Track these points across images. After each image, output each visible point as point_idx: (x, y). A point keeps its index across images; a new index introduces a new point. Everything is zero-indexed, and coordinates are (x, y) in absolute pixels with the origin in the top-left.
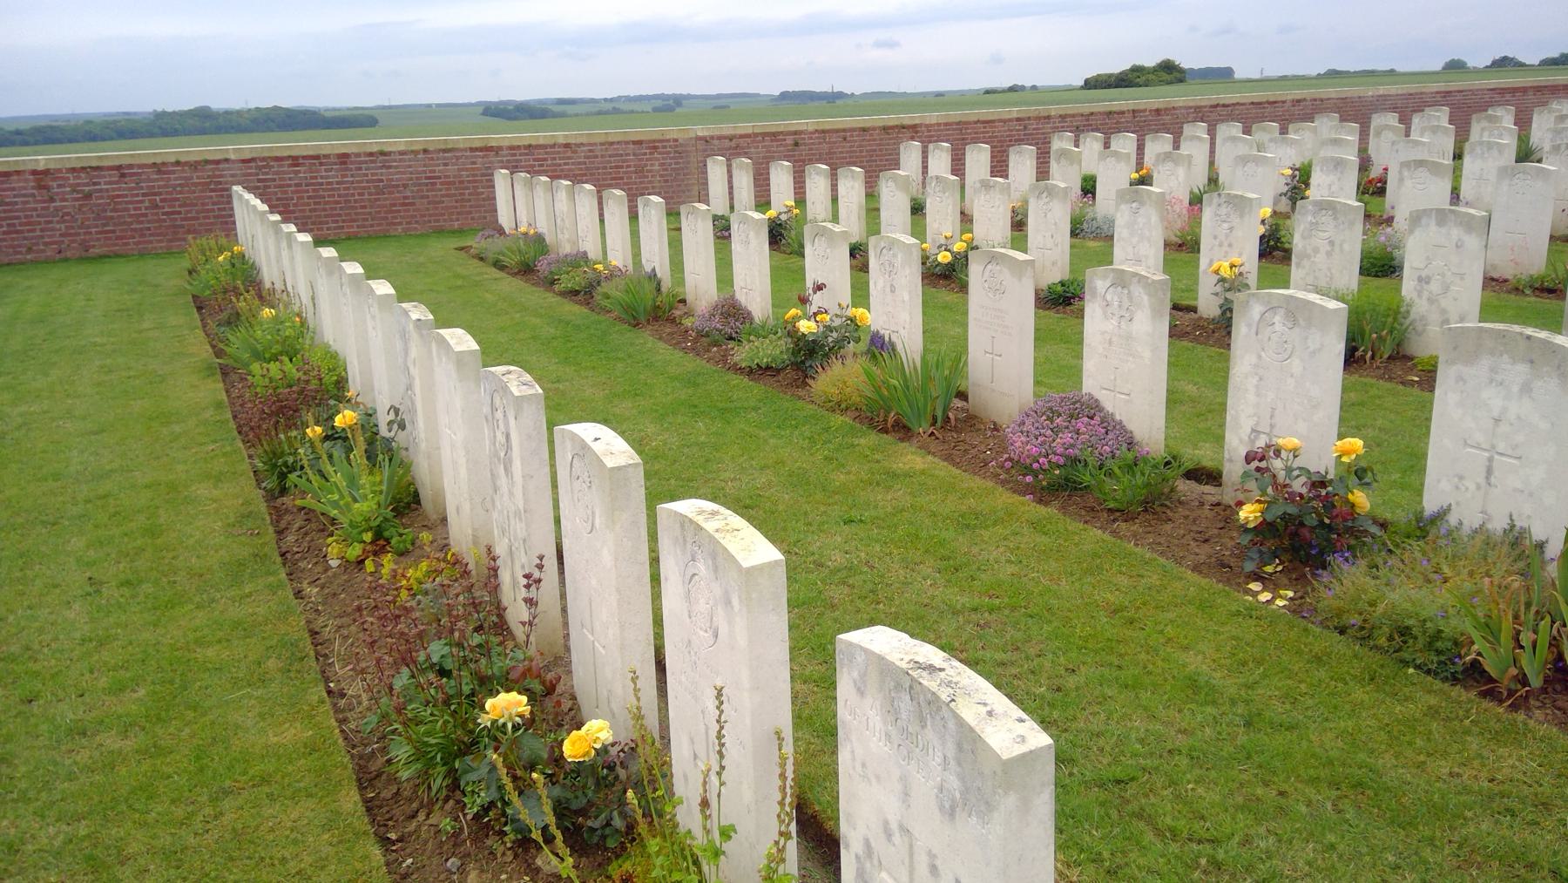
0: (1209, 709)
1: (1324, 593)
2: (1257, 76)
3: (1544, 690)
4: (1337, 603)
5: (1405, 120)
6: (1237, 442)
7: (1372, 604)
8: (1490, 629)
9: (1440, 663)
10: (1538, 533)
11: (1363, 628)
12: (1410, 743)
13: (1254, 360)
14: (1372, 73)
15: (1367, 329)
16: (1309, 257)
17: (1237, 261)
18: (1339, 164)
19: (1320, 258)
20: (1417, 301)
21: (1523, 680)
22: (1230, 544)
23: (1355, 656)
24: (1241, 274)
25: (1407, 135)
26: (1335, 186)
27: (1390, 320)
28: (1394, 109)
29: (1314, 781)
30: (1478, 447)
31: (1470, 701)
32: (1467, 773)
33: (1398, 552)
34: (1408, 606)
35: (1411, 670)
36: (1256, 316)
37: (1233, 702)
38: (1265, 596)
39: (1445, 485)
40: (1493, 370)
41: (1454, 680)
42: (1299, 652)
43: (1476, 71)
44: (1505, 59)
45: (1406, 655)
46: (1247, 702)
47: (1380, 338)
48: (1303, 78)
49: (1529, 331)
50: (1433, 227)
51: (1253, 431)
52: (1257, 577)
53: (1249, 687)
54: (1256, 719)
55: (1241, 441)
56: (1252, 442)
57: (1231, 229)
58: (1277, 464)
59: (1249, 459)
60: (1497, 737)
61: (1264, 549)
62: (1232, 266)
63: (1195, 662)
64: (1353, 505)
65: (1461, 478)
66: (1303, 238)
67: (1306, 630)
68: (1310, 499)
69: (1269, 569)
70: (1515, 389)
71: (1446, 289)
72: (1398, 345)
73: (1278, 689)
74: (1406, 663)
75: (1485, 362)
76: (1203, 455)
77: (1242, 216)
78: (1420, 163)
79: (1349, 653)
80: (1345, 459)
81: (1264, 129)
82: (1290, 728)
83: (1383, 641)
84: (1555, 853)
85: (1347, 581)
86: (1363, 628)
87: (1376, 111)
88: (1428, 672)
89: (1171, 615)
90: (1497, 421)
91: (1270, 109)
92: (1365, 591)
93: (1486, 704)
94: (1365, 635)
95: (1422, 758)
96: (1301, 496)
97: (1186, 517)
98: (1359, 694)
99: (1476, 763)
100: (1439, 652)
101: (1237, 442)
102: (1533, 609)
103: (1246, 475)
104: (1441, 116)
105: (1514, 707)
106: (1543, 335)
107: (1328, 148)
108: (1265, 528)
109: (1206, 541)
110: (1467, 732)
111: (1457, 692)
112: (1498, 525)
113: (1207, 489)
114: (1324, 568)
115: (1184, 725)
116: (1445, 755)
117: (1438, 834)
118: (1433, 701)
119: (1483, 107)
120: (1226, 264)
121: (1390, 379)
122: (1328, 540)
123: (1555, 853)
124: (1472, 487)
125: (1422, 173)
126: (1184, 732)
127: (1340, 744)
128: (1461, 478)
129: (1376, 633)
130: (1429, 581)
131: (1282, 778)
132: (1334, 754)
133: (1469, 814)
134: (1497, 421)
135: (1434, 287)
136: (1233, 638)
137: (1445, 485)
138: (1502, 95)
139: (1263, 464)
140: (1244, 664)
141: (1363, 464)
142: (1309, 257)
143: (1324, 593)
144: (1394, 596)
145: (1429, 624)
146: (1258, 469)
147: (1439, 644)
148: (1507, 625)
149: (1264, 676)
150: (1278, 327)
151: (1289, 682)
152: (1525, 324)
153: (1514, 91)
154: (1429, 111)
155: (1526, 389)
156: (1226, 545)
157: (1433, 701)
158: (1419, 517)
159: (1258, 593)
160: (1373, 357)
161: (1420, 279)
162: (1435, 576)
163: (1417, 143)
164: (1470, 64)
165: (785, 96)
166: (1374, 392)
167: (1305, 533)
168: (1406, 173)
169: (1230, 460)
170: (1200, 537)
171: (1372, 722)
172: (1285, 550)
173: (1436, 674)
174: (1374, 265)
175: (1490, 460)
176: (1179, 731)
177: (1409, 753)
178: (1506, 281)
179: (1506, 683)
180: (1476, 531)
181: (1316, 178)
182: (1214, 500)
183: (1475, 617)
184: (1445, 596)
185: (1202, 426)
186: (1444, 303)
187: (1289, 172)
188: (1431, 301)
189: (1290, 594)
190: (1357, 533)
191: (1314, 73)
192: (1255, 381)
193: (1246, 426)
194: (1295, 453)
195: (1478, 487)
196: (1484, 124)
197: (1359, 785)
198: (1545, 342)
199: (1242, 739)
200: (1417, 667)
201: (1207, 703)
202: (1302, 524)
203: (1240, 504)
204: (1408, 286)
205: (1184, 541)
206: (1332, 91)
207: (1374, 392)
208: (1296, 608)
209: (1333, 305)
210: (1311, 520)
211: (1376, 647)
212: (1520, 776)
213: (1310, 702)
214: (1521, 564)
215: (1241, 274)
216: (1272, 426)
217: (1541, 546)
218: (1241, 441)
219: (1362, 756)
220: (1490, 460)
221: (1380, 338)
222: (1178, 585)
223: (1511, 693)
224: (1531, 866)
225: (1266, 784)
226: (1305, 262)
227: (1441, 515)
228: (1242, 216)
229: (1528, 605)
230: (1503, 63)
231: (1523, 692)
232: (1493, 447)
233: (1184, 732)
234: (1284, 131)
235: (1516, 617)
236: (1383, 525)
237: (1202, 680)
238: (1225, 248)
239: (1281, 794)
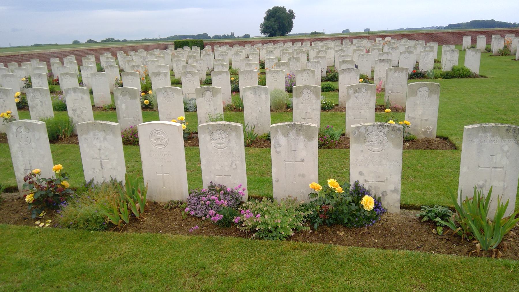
0: (27, 270)
1: (60, 217)
2: (9, 46)
3: (130, 223)
4: (65, 219)
5: (61, 60)
6: (20, 175)
7: (76, 215)
8: (111, 211)
9: (100, 226)
10: (119, 179)
11: (75, 224)
12: (95, 254)
13: (18, 145)
14: (50, 45)
15: (60, 128)
16: (35, 107)
17: (9, 112)
18: (40, 76)
19: (39, 107)
20: (74, 117)
21: (124, 222)
22: (26, 211)
23: (74, 233)
24: (12, 116)
25: (63, 64)
26: (41, 84)
27: (67, 124)
28: (57, 57)
29: (68, 278)
30: (96, 159)
31: (111, 234)
32: (114, 255)
33: (81, 197)
34: (86, 212)
35: (92, 232)
36: (15, 131)
37: (36, 264)
38: (42, 224)
39: (90, 172)
40: (94, 135)
41: (106, 229)
42: (56, 239)
43: (83, 44)
44: (90, 40)
45: (90, 228)
46: (41, 262)
47: (65, 130)
48: (26, 47)
49: (101, 122)
50: (73, 94)
51: (25, 170)
52: (38, 219)
53: (41, 257)
54: (45, 266)
55: (21, 174)
56: (26, 173)
57: (4, 101)
58: (35, 179)
59: (25, 180)
60: (120, 242)
61: (38, 209)
62: (8, 114)
63: (20, 256)
64: (64, 186)
65: (94, 169)
66: (31, 101)
67: (57, 231)
68: (49, 188)
69: (41, 215)
70: (102, 139)
71: (82, 112)
72: (72, 132)
73: (50, 254)
74: (90, 230)
75: (92, 133)
76: (11, 183)
77: (7, 96)
78: (67, 74)
79: (72, 233)
80: (57, 172)
81: (12, 65)
82: (57, 265)
83: (82, 226)
84: (140, 268)
85: (67, 211)
86: (75, 224)
87: (51, 57)
88: (97, 230)
89: (7, 243)
90: (100, 150)
91: (13, 58)
92: (72, 212)
93: (116, 233)
94: (76, 226)
95: (100, 257)
96: (46, 187)
97: (8, 206)
98: (78, 245)
99: (115, 252)
100: (99, 223)
101: (20, 175)
102: (122, 201)
103: (24, 186)
104: (73, 59)
105: (123, 231)
106: (105, 122)
107: (37, 71)
108: (36, 202)
109: (17, 212)
110: (111, 243)
111: (107, 233)
112: (108, 180)
113: (14, 194)
114: (59, 209)
115: (19, 279)
116: (106, 253)
117: (108, 277)
118: (100, 238)
119: (85, 55)
120: (5, 113)
121: (72, 143)
122: (58, 199)
123: (140, 268)
124: (98, 171)
125: (68, 77)
126: (20, 282)
127: (74, 263)
128: (94, 169)
129: (79, 224)
130: (92, 203)
131: (57, 282)
132: (72, 267)
133: (115, 267)
134: (100, 150)
135: (78, 112)
136: (33, 242)
137: (90, 172)
138: (73, 53)
139: (31, 180)
140: (38, 250)
141: (64, 172)
142: (35, 107)
143: (60, 217)
144: (82, 211)
145: (94, 216)
146: (30, 183)
147: (98, 221)
148: (115, 208)
149: (45, 251)
150: (23, 133)
151: (54, 250)
152: (107, 120)
153: (93, 50)
154: (69, 57)
155: (105, 139)
156: (24, 212)
157: (100, 238)
158: (86, 185)
159: (39, 224)
160: (65, 137)
161: (73, 110)
162: (93, 201)
163: (65, 67)
164: (81, 42)
165: (136, 41)
166: (67, 148)
167: (50, 199)
168: (63, 77)
169: (19, 182)
170: (14, 212)
171: (83, 252)
172: (45, 207)
173: (100, 230)
174: (60, 107)
175: (101, 161)
176: (18, 282)
177: (96, 257)
178: (102, 107)
179: (119, 225)
180: (102, 184)
181: (33, 80)
182: (18, 197)
183: (107, 209)
184: (97, 206)
185: (9, 172)
186: (82, 117)
187: (25, 79)
188: (78, 116)
189: (50, 221)
190: (68, 195)
191: (30, 45)
192: (20, 153)
193: (22, 168)
194: (39, 174)
195: (100, 170)
196: (86, 60)
197: (82, 273)
198: (106, 124)
199: (41, 275)
200: (94, 230)
201: (26, 268)
202: (48, 197)
203: (25, 196)
204: (70, 112)
205: (9, 215)
206: (35, 51)
207: (67, 148)
208: (53, 225)
209: (40, 123)
210: (51, 195)
211: (80, 228)
212: (128, 250)
213: (62, 254)
214: (116, 190)
215: (12, 116)
216: (31, 167)
217: (121, 183)
218: (21, 174)
219: (82, 264)
220: (101, 161)
221: (65, 130)
222: (9, 231)
223: (122, 227)
224: (134, 275)
225: (52, 286)
226: (34, 109)
227: (91, 182)
228: (7, 96)
229: (120, 201)
230: (90, 42)
231: (125, 226)
232: (101, 157)
233: (20, 282)
234: (20, 65)
235: (118, 205)
236: (75, 190)
237: (23, 262)
238: (4, 108)
239: (57, 287)
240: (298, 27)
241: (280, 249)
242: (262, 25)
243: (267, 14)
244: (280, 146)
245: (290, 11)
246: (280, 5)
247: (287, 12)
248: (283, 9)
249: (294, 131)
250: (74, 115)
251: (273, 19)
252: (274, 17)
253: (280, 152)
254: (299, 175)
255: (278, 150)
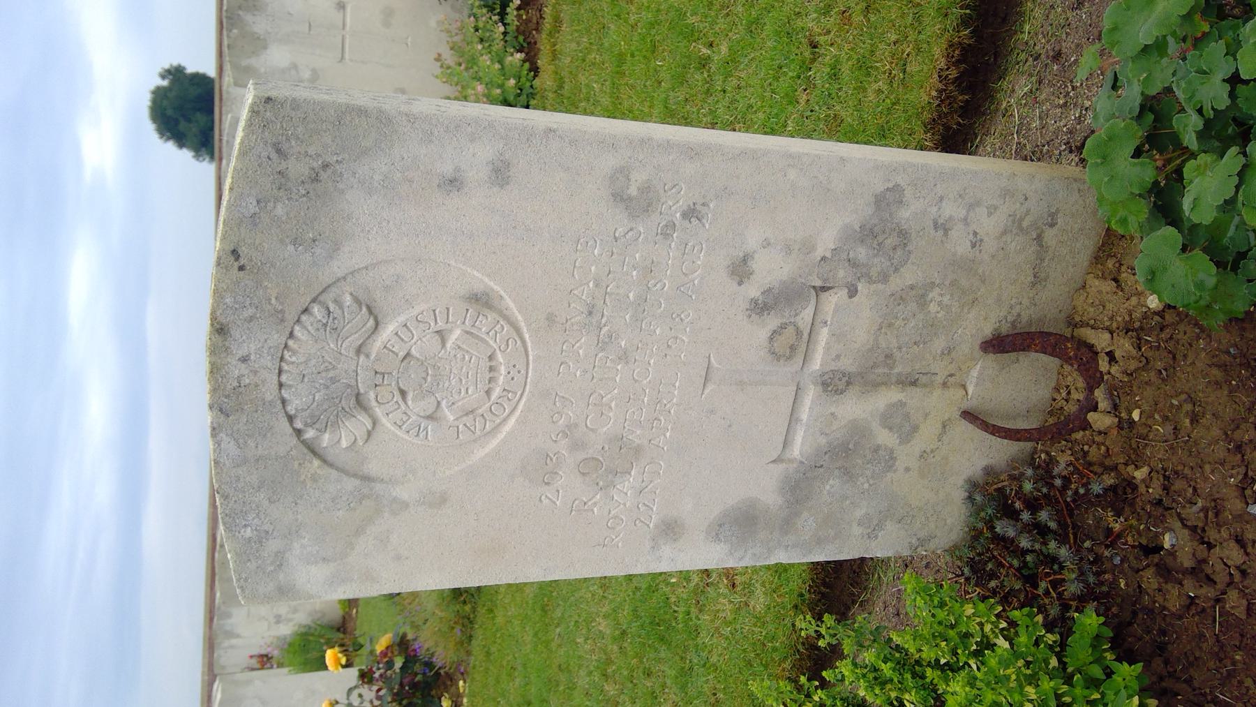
83: (468, 608)
98: (500, 620)
189: (461, 683)
240: (202, 62)
241: (551, 95)
242: (198, 156)
243: (169, 139)
244: (295, 66)
245: (163, 77)
246: (146, 101)
247: (165, 83)
248: (159, 97)
249: (248, 18)
250: (290, 620)
251: (183, 125)
252: (177, 122)
253: (314, 71)
254: (387, 24)
255: (306, 75)
